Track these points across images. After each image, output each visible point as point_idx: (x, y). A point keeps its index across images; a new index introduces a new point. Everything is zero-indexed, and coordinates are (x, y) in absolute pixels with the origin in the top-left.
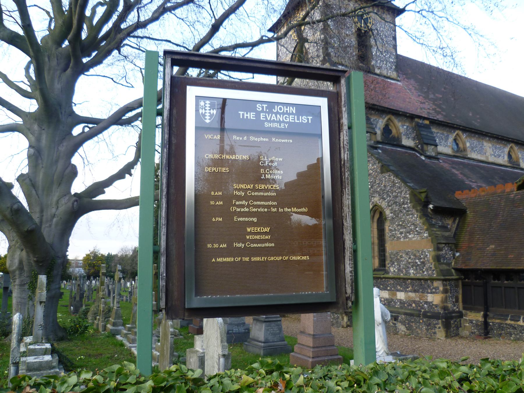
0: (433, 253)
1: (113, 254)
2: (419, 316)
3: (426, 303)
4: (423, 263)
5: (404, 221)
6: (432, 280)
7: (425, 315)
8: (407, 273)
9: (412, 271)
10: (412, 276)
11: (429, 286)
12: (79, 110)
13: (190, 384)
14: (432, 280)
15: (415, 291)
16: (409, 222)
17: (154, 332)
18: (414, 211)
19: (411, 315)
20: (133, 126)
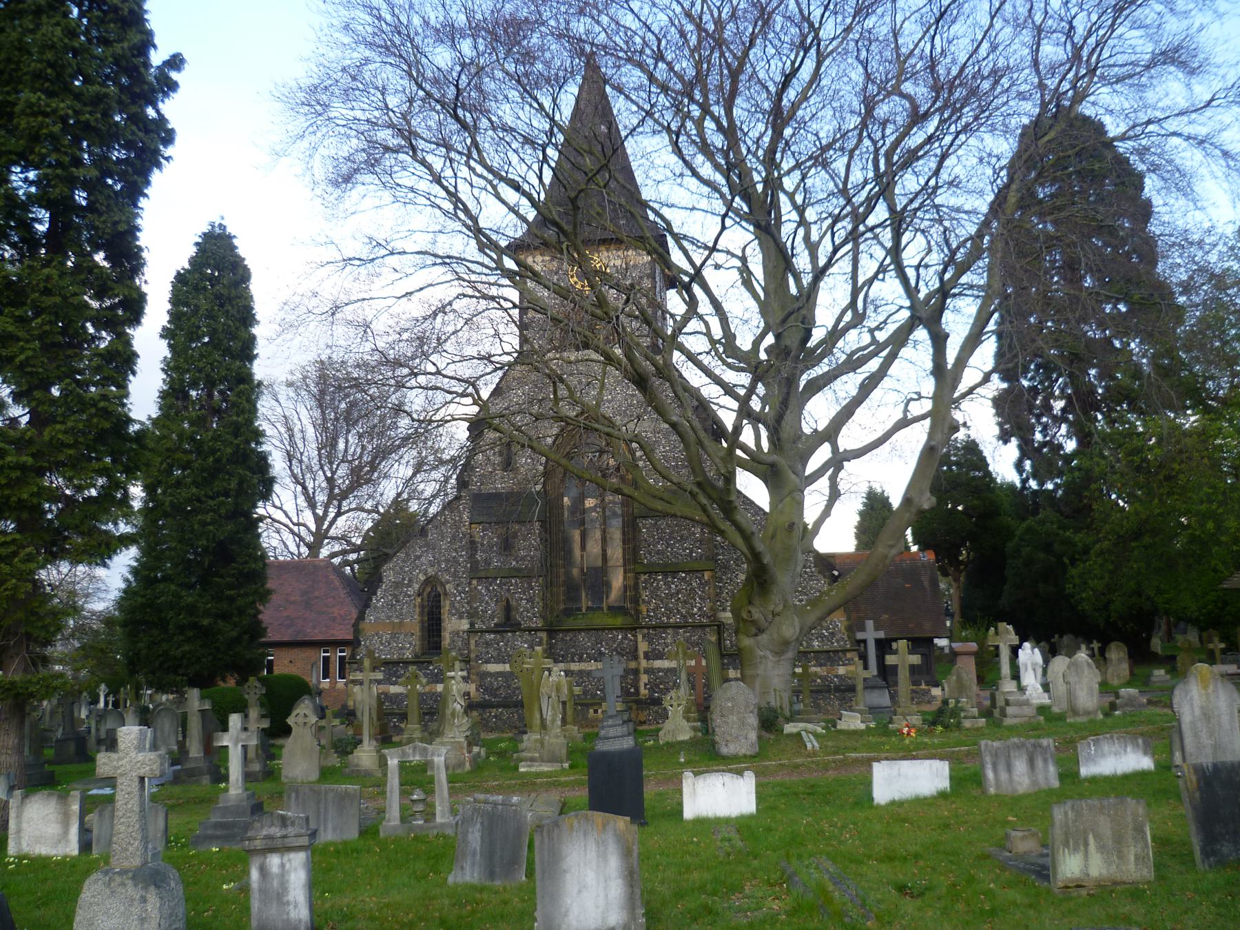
0: (846, 623)
1: (143, 202)
2: (829, 691)
3: (837, 676)
4: (833, 634)
5: (805, 587)
6: (845, 651)
7: (837, 689)
8: (809, 645)
9: (816, 643)
10: (817, 648)
11: (840, 659)
12: (133, 415)
13: (106, 340)
14: (845, 651)
15: (821, 665)
16: (812, 588)
17: (323, 742)
18: (820, 576)
19: (818, 692)
20: (793, 255)
